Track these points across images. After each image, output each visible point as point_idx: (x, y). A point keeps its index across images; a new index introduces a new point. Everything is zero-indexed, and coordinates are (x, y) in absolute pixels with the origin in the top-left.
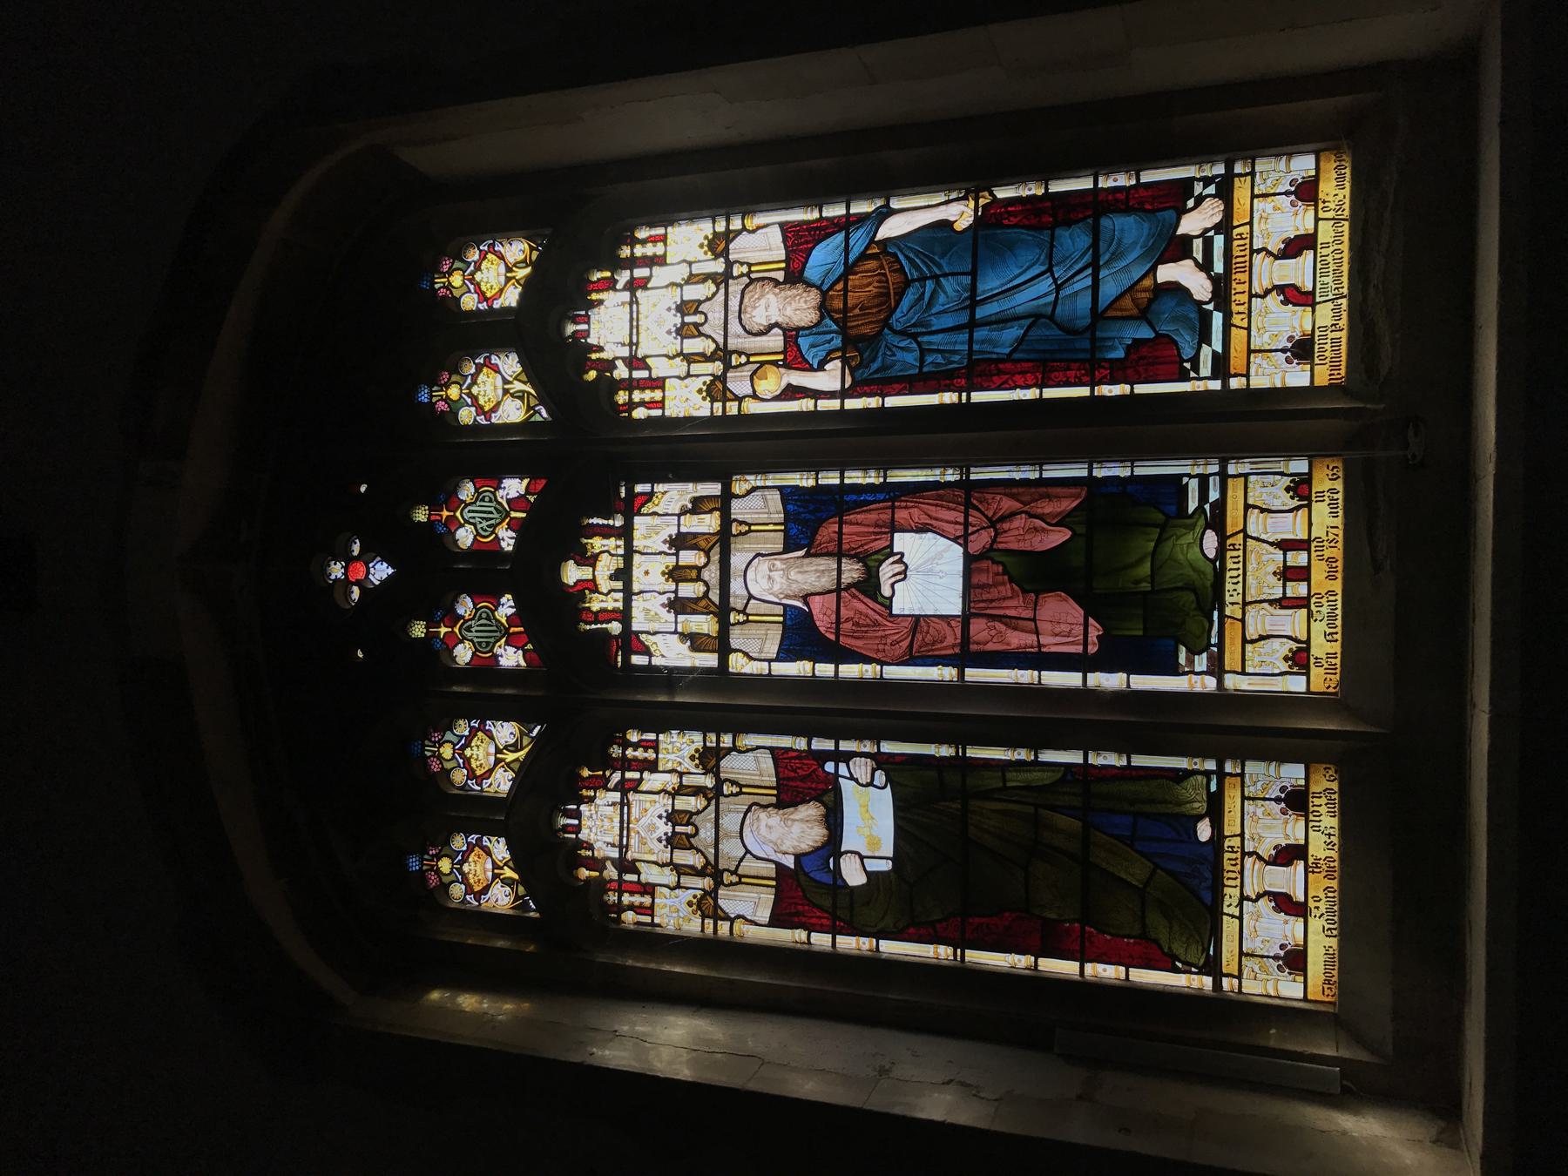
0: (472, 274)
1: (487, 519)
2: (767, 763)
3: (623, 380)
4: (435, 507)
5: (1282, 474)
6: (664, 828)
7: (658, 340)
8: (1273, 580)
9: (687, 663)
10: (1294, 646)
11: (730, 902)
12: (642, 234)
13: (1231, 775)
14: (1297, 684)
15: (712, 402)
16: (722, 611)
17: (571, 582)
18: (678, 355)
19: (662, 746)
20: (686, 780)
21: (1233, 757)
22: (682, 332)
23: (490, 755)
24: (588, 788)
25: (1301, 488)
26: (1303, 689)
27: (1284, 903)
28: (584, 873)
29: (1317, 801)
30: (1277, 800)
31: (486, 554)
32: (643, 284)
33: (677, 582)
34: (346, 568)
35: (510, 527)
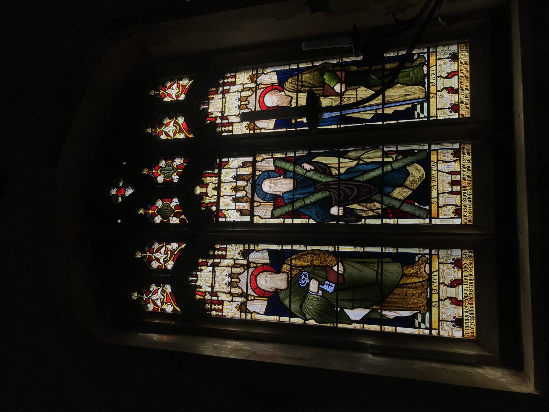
2: (266, 254)
3: (219, 123)
4: (143, 251)
6: (227, 280)
7: (221, 285)
8: (447, 185)
9: (239, 220)
11: (251, 306)
12: (218, 246)
13: (434, 254)
14: (458, 221)
18: (228, 293)
19: (228, 249)
20: (237, 262)
22: (231, 284)
25: (457, 154)
28: (198, 297)
30: (451, 263)
31: (161, 270)
33: (236, 191)
35: (177, 175)
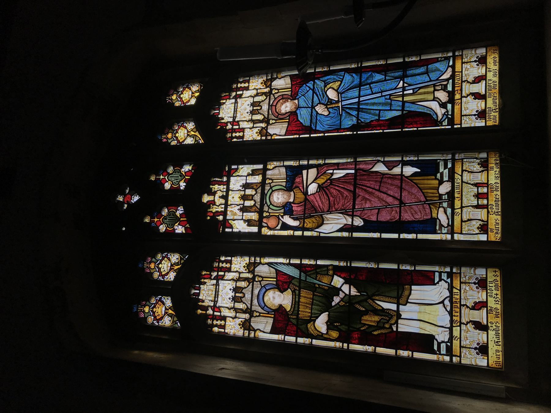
0: (180, 95)
1: (177, 179)
5: (477, 158)
6: (231, 294)
8: (473, 198)
9: (247, 231)
10: (481, 223)
14: (483, 238)
15: (244, 330)
16: (260, 212)
17: (205, 202)
19: (233, 262)
21: (457, 266)
22: (253, 113)
23: (167, 266)
24: (223, 100)
25: (485, 165)
26: (486, 365)
27: (478, 326)
28: (199, 311)
29: (491, 285)
31: (175, 190)
32: (240, 96)
33: (244, 200)
34: (124, 198)
35: (185, 182)
